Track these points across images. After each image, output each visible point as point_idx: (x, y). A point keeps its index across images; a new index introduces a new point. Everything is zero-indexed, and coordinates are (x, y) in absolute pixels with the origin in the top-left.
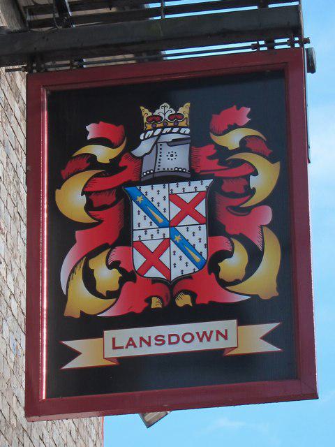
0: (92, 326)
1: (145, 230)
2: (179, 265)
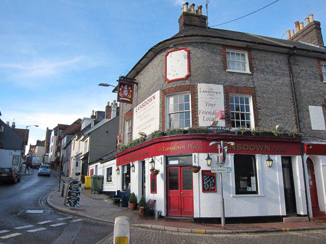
0: (121, 97)
1: (124, 92)
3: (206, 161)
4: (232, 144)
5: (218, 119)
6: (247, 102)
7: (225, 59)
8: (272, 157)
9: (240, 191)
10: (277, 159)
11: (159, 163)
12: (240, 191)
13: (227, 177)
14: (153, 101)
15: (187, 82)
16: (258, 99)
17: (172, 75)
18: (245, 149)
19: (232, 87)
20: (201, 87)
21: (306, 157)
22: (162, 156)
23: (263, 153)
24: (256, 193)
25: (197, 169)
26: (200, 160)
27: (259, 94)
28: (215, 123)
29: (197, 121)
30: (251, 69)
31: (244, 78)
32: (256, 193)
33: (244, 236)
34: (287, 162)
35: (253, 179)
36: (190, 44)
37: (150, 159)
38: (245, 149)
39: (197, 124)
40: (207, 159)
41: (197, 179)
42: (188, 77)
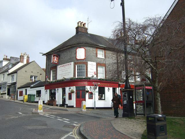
3: (128, 18)
4: (99, 83)
5: (94, 75)
6: (84, 67)
7: (97, 53)
8: (110, 88)
9: (100, 99)
10: (111, 89)
11: (74, 88)
12: (100, 99)
13: (96, 95)
14: (69, 65)
15: (84, 61)
17: (79, 57)
18: (102, 85)
19: (99, 63)
20: (89, 63)
21: (120, 88)
22: (75, 87)
23: (107, 86)
24: (104, 100)
25: (88, 92)
26: (88, 88)
27: (107, 66)
28: (93, 77)
29: (87, 75)
31: (102, 60)
32: (104, 100)
33: (101, 46)
34: (114, 90)
35: (103, 95)
36: (86, 46)
37: (69, 88)
38: (102, 85)
39: (63, 89)
40: (129, 19)
41: (87, 95)
42: (85, 58)
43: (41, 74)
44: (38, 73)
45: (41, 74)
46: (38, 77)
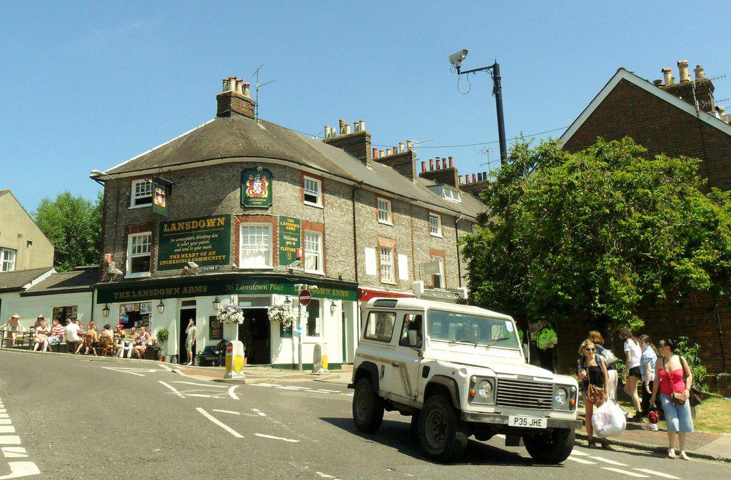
1: (255, 188)
2: (258, 192)
16: (327, 237)
30: (323, 204)
37: (213, 298)
43: (30, 243)
44: (20, 236)
45: (30, 243)
46: (20, 252)
